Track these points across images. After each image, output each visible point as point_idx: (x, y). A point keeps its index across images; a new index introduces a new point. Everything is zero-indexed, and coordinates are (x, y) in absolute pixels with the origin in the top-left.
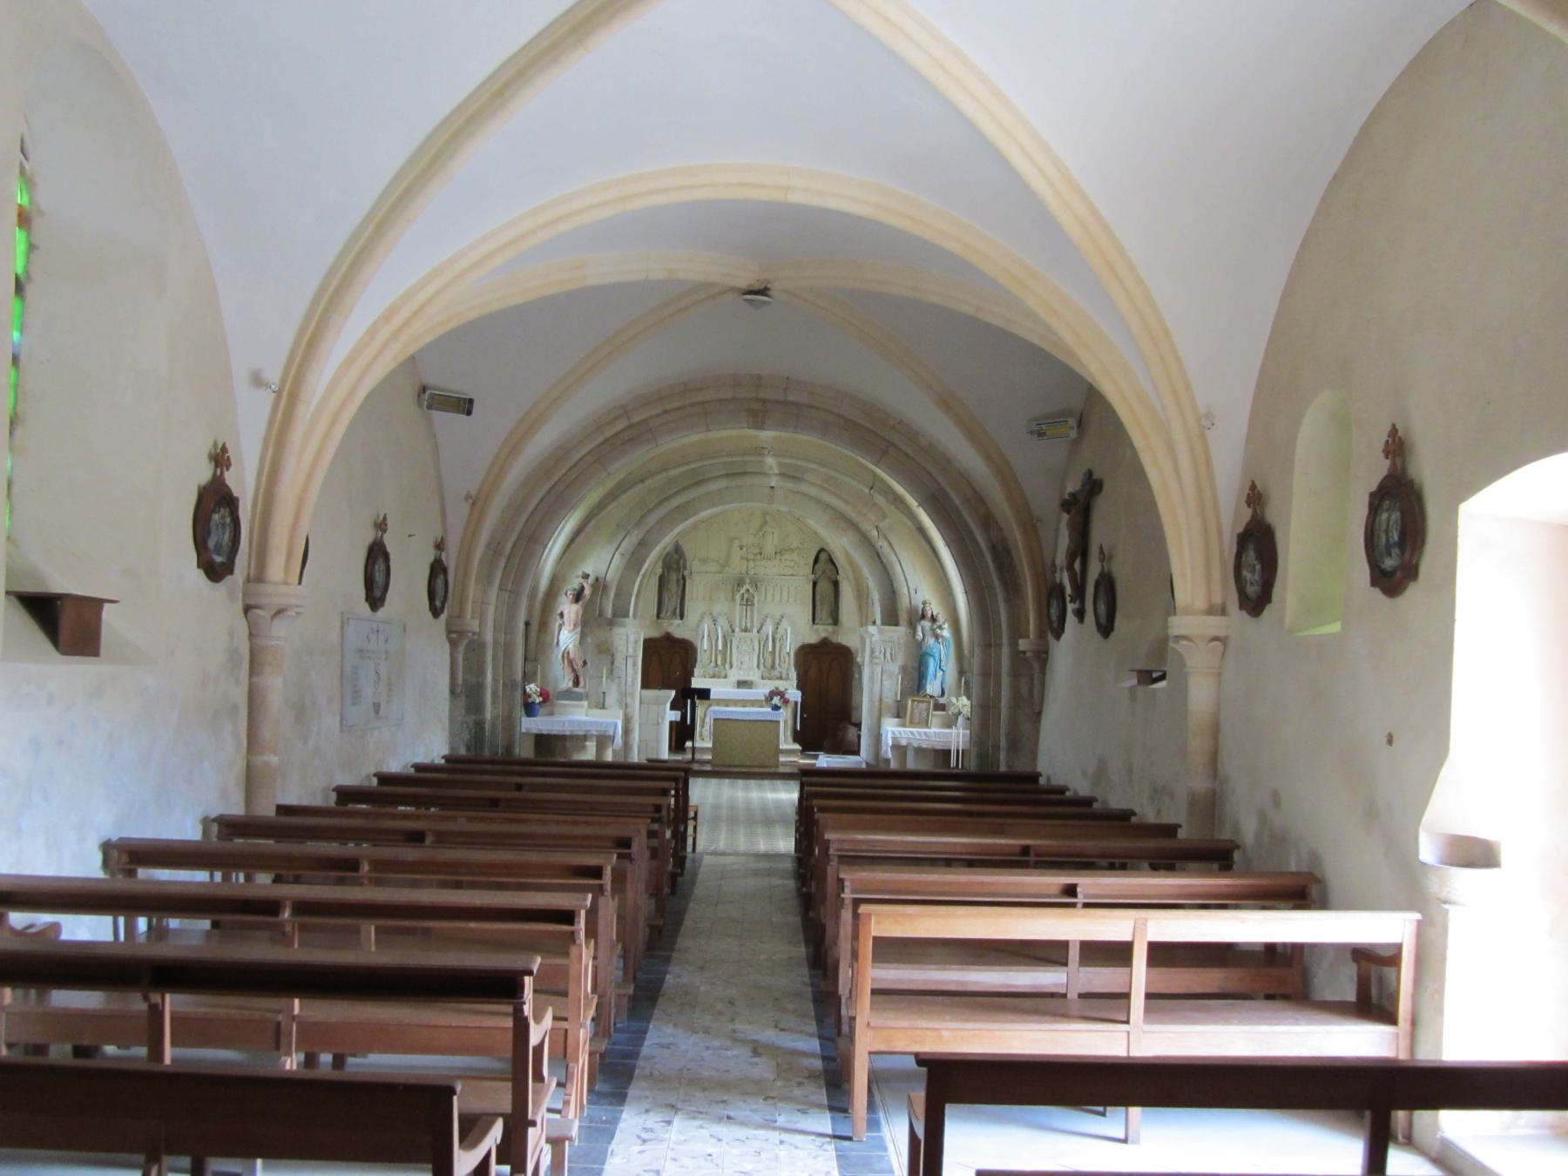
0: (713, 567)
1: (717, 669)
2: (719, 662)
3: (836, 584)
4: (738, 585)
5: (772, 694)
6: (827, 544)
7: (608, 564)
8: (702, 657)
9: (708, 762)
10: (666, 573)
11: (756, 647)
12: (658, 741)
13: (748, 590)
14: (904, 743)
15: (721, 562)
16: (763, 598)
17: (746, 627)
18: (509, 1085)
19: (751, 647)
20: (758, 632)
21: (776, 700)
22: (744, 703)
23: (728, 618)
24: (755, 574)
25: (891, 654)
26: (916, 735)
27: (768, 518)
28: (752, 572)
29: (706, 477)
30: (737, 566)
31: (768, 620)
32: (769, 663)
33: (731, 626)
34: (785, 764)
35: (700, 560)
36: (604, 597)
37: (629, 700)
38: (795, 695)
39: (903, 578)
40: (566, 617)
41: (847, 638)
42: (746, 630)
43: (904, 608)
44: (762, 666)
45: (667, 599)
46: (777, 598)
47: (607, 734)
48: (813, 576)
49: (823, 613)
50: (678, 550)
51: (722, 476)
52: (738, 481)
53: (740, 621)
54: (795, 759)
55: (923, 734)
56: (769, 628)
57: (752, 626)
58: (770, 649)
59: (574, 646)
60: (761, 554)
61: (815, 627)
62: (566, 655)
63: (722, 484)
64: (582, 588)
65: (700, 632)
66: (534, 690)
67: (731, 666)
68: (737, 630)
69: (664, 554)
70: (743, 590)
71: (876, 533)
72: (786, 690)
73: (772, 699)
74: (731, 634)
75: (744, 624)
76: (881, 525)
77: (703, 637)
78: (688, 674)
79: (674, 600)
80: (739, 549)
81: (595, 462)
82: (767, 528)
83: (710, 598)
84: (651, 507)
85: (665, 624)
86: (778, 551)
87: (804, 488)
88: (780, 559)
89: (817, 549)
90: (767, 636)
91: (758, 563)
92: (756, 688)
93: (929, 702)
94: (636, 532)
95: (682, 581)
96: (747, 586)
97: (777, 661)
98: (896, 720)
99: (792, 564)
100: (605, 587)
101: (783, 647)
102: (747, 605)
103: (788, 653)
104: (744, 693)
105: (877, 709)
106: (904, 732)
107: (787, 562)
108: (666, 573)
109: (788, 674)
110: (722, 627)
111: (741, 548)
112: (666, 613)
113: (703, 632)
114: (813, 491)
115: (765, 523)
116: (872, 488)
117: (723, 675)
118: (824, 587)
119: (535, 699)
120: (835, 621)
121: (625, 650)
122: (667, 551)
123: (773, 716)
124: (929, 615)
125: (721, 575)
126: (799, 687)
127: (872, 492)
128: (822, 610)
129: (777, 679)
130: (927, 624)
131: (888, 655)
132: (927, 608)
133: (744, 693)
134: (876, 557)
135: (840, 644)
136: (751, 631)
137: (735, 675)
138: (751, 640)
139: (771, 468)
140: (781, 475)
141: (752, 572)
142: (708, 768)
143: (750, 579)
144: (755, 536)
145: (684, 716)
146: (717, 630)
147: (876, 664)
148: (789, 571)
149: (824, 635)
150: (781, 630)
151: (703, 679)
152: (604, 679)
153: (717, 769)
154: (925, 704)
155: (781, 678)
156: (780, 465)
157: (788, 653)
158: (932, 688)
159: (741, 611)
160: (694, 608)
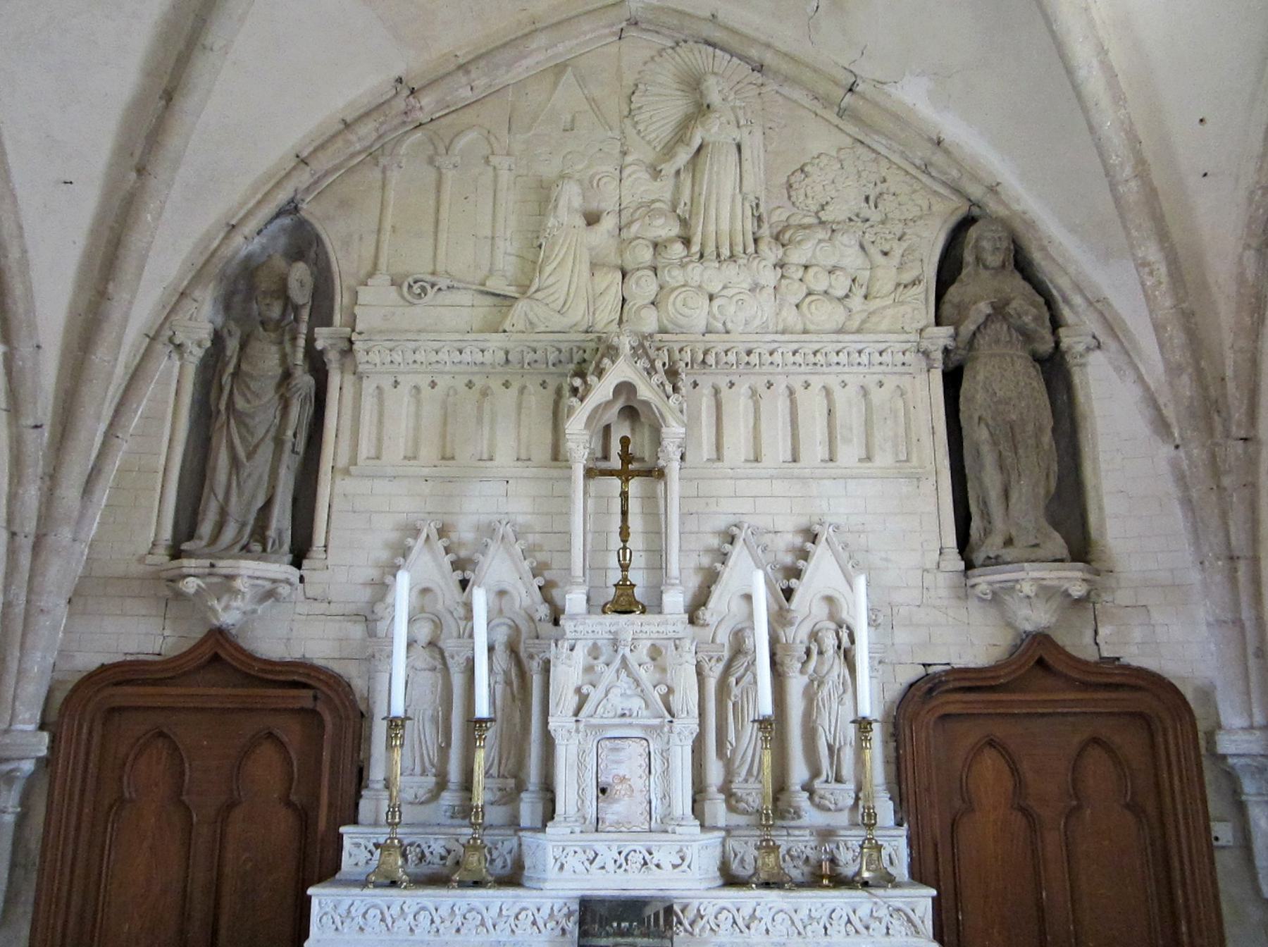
11: (686, 696)
17: (624, 586)
31: (739, 554)
32: (755, 793)
42: (624, 603)
61: (984, 581)
68: (575, 600)
70: (602, 390)
74: (547, 628)
80: (580, 222)
82: (714, 130)
90: (739, 649)
95: (304, 381)
96: (620, 371)
97: (798, 772)
112: (220, 527)
115: (702, 109)
136: (654, 606)
144: (656, 173)
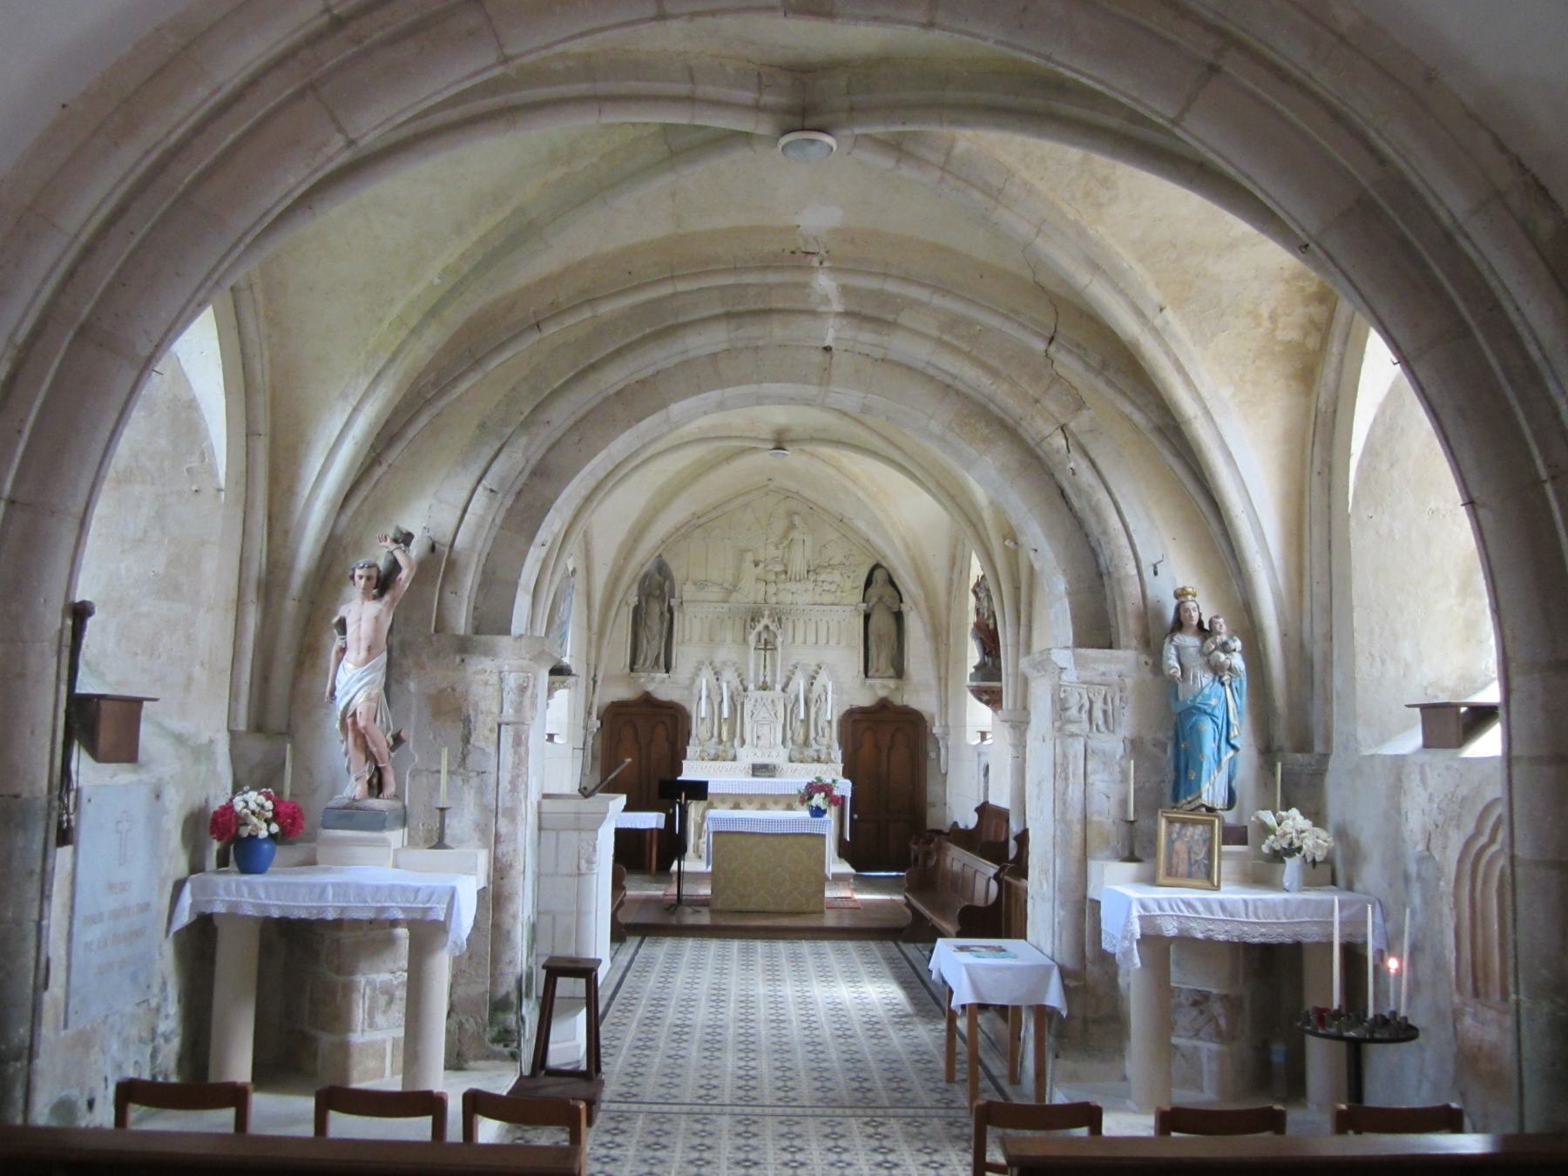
0: (714, 593)
1: (721, 747)
2: (725, 737)
3: (899, 617)
4: (753, 620)
5: (812, 789)
6: (884, 557)
7: (459, 513)
8: (699, 731)
9: (703, 903)
10: (644, 603)
12: (580, 913)
13: (767, 627)
14: (1170, 929)
15: (726, 585)
16: (790, 640)
17: (765, 682)
18: (709, 791)
19: (773, 713)
20: (783, 690)
21: (818, 800)
22: (763, 801)
23: (736, 671)
24: (777, 603)
25: (1105, 712)
26: (1200, 908)
27: (797, 520)
28: (773, 600)
29: (682, 319)
30: (751, 591)
32: (800, 739)
33: (741, 682)
34: (838, 906)
35: (695, 584)
36: (448, 589)
37: (504, 826)
38: (844, 788)
39: (1124, 541)
40: (350, 629)
41: (920, 697)
42: (764, 687)
43: (1130, 608)
44: (789, 743)
45: (645, 641)
46: (811, 639)
47: (432, 916)
48: (863, 606)
49: (881, 661)
50: (662, 568)
51: (716, 318)
52: (752, 331)
53: (757, 675)
54: (846, 893)
55: (1216, 908)
56: (799, 683)
57: (774, 682)
58: (802, 716)
59: (369, 699)
60: (786, 573)
61: (869, 681)
62: (349, 721)
63: (713, 339)
64: (395, 567)
65: (695, 691)
66: (253, 806)
67: (743, 742)
68: (751, 687)
69: (642, 573)
70: (760, 627)
71: (1064, 442)
72: (834, 781)
73: (811, 798)
75: (762, 679)
76: (1072, 425)
77: (700, 698)
78: (676, 757)
79: (655, 643)
81: (300, 94)
82: (796, 535)
83: (711, 640)
84: (556, 385)
85: (642, 680)
86: (812, 568)
87: (901, 345)
88: (815, 581)
89: (871, 566)
91: (781, 586)
92: (781, 777)
93: (1212, 824)
94: (523, 440)
96: (765, 621)
97: (812, 734)
98: (1131, 868)
99: (833, 588)
100: (452, 565)
101: (820, 714)
102: (765, 649)
103: (830, 722)
104: (763, 785)
105: (1077, 840)
106: (1170, 901)
107: (830, 580)
108: (644, 603)
109: (829, 754)
110: (728, 683)
111: (756, 565)
113: (700, 691)
114: (919, 352)
115: (792, 526)
116: (1051, 340)
117: (730, 755)
118: (881, 621)
119: (256, 828)
120: (899, 672)
121: (496, 710)
122: (645, 569)
123: (815, 826)
124: (1195, 622)
125: (726, 605)
126: (846, 774)
127: (1052, 348)
128: (878, 656)
129: (814, 761)
130: (1189, 641)
131: (1098, 715)
132: (1191, 605)
133: (763, 785)
134: (1059, 501)
135: (906, 707)
137: (748, 756)
138: (773, 701)
139: (826, 300)
140: (847, 314)
141: (773, 600)
142: (705, 919)
143: (771, 610)
144: (777, 547)
145: (670, 820)
146: (720, 688)
147: (1072, 735)
148: (828, 598)
149: (882, 693)
150: (817, 687)
151: (700, 763)
152: (444, 776)
153: (722, 922)
154: (1200, 828)
155: (818, 760)
156: (845, 291)
157: (830, 722)
158: (1212, 790)
159: (758, 658)
160: (686, 655)
